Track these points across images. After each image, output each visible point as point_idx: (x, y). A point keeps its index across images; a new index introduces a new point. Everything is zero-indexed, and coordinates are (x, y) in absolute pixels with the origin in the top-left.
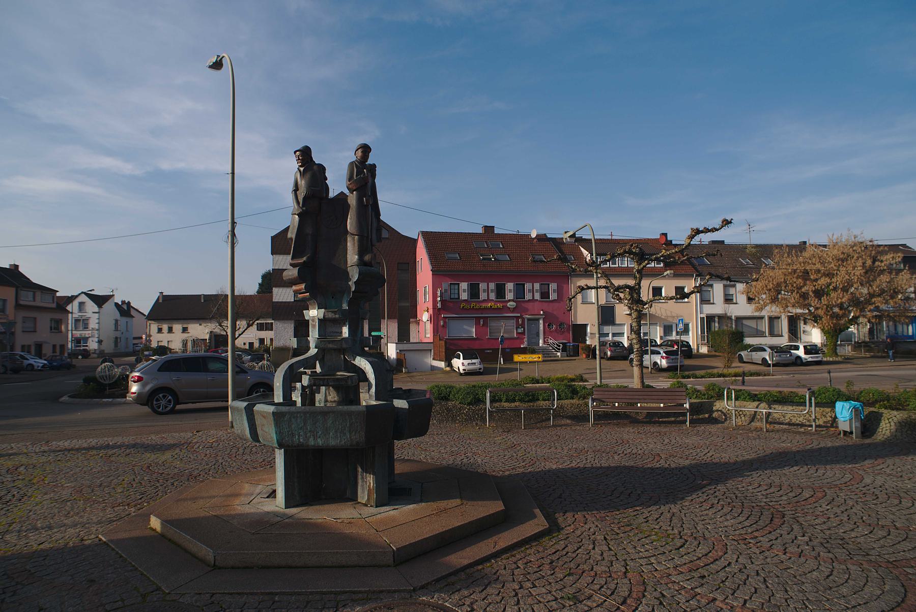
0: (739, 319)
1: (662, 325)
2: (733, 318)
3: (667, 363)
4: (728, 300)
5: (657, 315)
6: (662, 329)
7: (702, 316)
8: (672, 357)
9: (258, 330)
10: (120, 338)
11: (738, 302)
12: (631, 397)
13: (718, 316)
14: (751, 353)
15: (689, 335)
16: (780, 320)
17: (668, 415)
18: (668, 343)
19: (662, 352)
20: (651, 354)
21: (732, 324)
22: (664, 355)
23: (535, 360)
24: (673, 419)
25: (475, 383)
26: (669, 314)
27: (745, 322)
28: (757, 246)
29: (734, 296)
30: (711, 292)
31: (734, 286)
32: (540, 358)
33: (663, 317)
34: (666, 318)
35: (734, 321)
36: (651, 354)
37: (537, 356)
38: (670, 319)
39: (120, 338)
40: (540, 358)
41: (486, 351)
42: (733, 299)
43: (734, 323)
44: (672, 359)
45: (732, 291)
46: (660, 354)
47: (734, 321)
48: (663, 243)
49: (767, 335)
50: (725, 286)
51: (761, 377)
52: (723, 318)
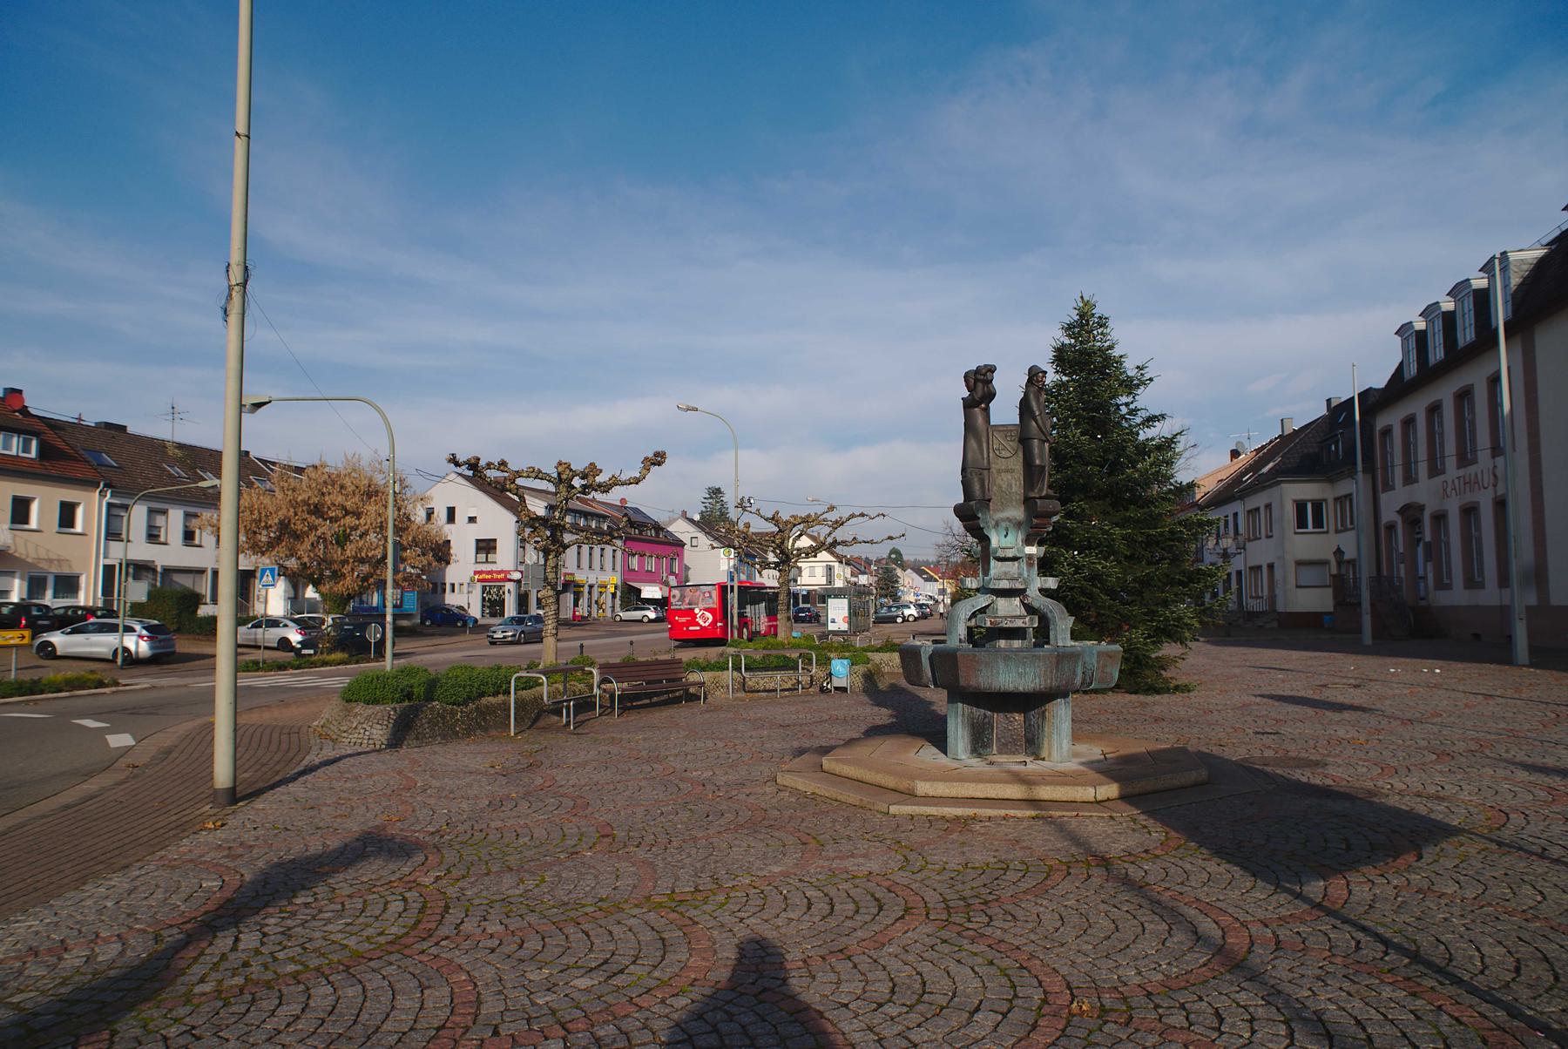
0: (168, 571)
1: (27, 578)
2: (159, 569)
3: (151, 648)
4: (153, 537)
5: (17, 554)
6: (25, 584)
7: (108, 562)
8: (161, 637)
9: (478, 541)
10: (1271, 567)
11: (169, 542)
12: (664, 671)
13: (134, 565)
14: (254, 630)
15: (77, 597)
16: (204, 576)
17: (638, 697)
18: (67, 612)
19: (138, 627)
20: (124, 631)
21: (156, 580)
22: (144, 632)
23: (12, 642)
24: (648, 701)
25: (498, 662)
26: (43, 555)
27: (178, 578)
28: (181, 446)
29: (163, 530)
30: (125, 519)
31: (165, 512)
32: (23, 637)
33: (29, 560)
34: (35, 561)
35: (159, 575)
36: (124, 631)
37: (17, 633)
38: (44, 566)
39: (1271, 567)
40: (23, 637)
41: (40, 622)
42: (159, 536)
43: (159, 579)
44: (160, 641)
45: (160, 520)
46: (134, 631)
47: (159, 575)
48: (17, 408)
49: (208, 601)
50: (151, 511)
51: (328, 668)
52: (140, 569)
